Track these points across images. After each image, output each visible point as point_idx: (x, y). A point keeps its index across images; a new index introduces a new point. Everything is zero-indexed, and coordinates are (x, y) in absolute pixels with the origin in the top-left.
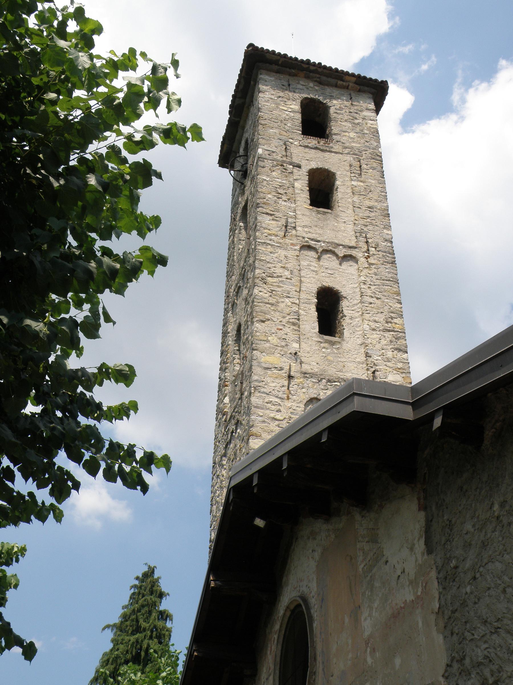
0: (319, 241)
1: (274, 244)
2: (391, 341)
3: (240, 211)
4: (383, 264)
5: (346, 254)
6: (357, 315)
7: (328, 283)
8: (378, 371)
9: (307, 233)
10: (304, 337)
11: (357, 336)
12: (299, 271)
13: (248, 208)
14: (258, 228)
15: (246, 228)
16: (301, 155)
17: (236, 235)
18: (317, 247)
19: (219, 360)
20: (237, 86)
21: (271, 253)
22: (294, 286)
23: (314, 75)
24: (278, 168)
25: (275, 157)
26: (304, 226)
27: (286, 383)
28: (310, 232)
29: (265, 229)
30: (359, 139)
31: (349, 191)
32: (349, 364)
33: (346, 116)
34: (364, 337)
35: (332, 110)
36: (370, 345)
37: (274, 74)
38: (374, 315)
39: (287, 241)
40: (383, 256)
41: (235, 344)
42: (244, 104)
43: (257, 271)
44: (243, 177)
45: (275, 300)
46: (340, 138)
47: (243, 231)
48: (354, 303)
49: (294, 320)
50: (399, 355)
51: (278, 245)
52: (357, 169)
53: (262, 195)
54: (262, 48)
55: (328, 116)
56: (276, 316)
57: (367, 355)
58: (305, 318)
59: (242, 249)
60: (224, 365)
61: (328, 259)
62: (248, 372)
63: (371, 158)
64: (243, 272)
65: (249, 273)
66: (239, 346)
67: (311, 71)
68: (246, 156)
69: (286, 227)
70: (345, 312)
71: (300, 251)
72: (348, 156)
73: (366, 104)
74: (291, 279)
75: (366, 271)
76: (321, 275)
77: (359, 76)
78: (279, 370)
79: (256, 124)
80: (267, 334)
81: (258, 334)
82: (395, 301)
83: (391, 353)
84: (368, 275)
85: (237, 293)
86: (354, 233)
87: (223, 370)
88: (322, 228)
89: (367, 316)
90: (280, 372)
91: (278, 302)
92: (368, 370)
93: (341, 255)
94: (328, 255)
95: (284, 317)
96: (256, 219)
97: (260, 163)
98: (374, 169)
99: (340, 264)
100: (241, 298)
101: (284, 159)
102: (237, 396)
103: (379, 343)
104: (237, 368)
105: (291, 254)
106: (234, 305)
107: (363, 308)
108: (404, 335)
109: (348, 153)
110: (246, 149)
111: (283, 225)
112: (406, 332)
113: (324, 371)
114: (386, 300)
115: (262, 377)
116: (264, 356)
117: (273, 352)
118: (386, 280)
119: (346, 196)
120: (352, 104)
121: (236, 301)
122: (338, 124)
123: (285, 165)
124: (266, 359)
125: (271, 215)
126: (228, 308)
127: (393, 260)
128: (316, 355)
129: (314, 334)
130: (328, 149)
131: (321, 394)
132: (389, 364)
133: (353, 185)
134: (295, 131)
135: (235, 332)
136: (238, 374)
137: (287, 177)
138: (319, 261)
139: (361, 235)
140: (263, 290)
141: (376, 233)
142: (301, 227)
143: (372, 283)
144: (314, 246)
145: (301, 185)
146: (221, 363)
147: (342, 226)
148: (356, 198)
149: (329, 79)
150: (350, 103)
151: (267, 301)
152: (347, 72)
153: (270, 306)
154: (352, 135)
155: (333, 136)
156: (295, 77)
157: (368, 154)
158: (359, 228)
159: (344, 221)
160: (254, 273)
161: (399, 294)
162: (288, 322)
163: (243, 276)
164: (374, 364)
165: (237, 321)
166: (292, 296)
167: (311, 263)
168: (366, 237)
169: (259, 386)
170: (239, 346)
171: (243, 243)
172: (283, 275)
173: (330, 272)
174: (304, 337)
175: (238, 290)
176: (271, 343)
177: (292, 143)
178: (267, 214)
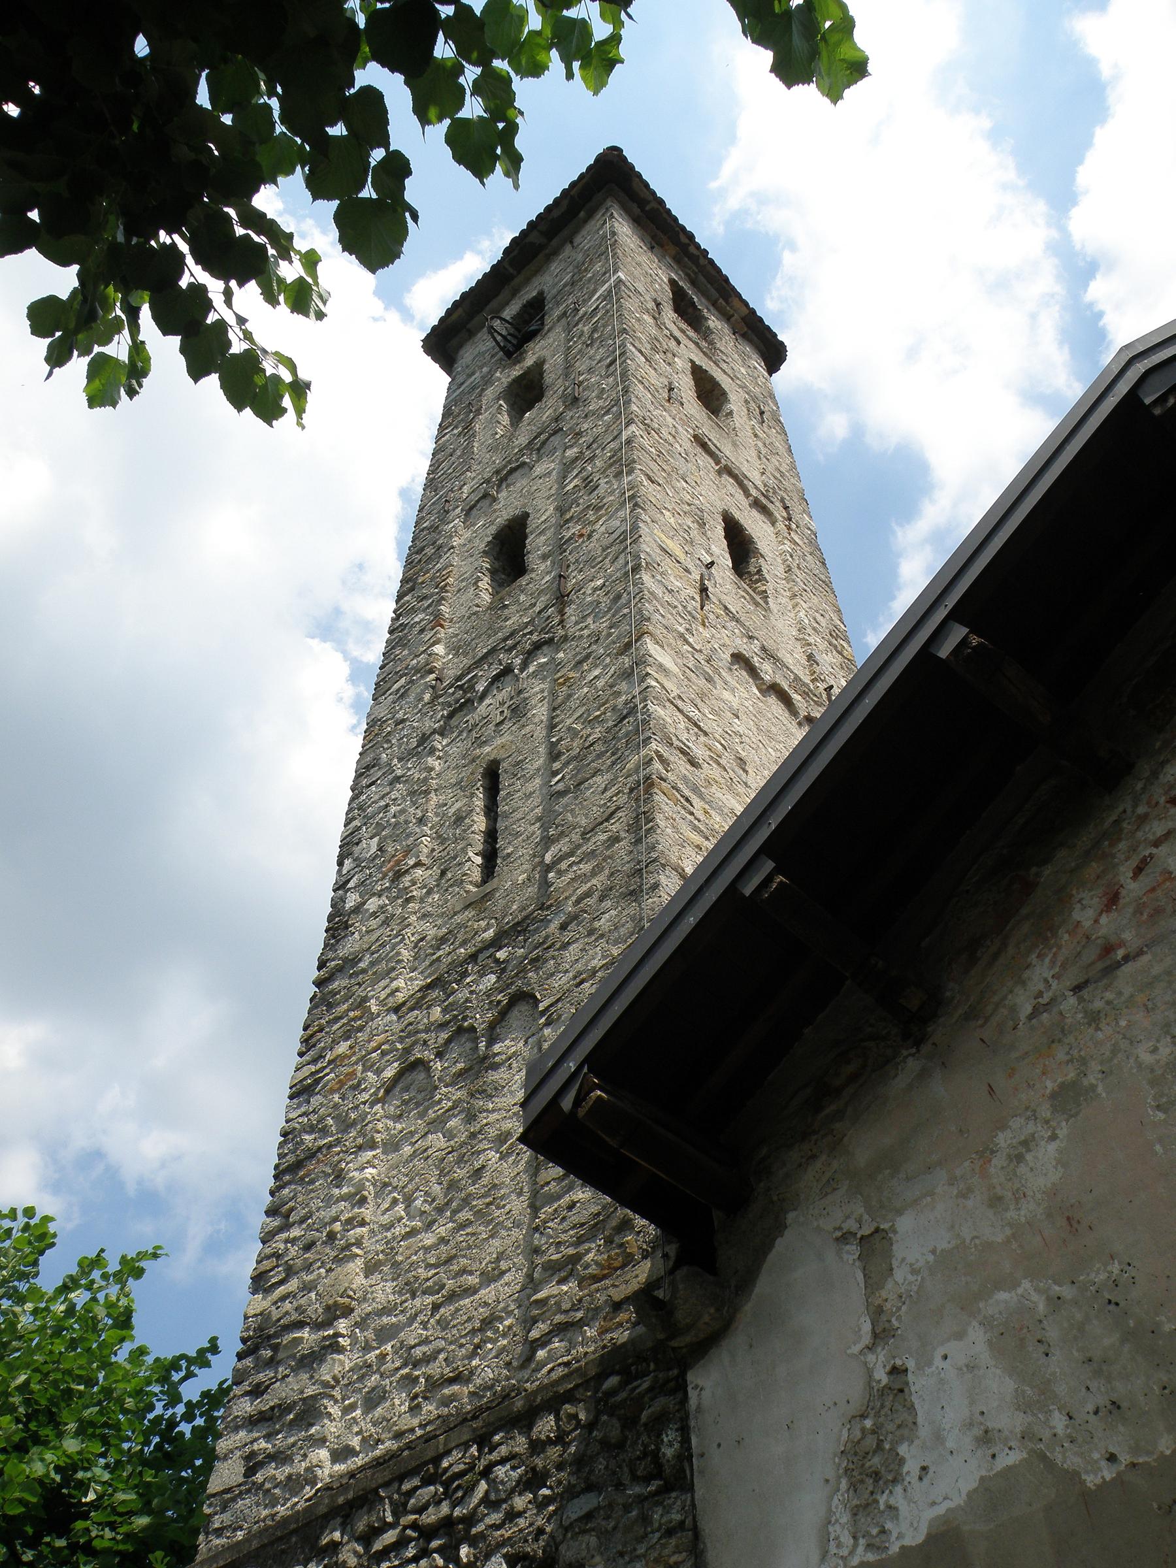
42: (541, 247)
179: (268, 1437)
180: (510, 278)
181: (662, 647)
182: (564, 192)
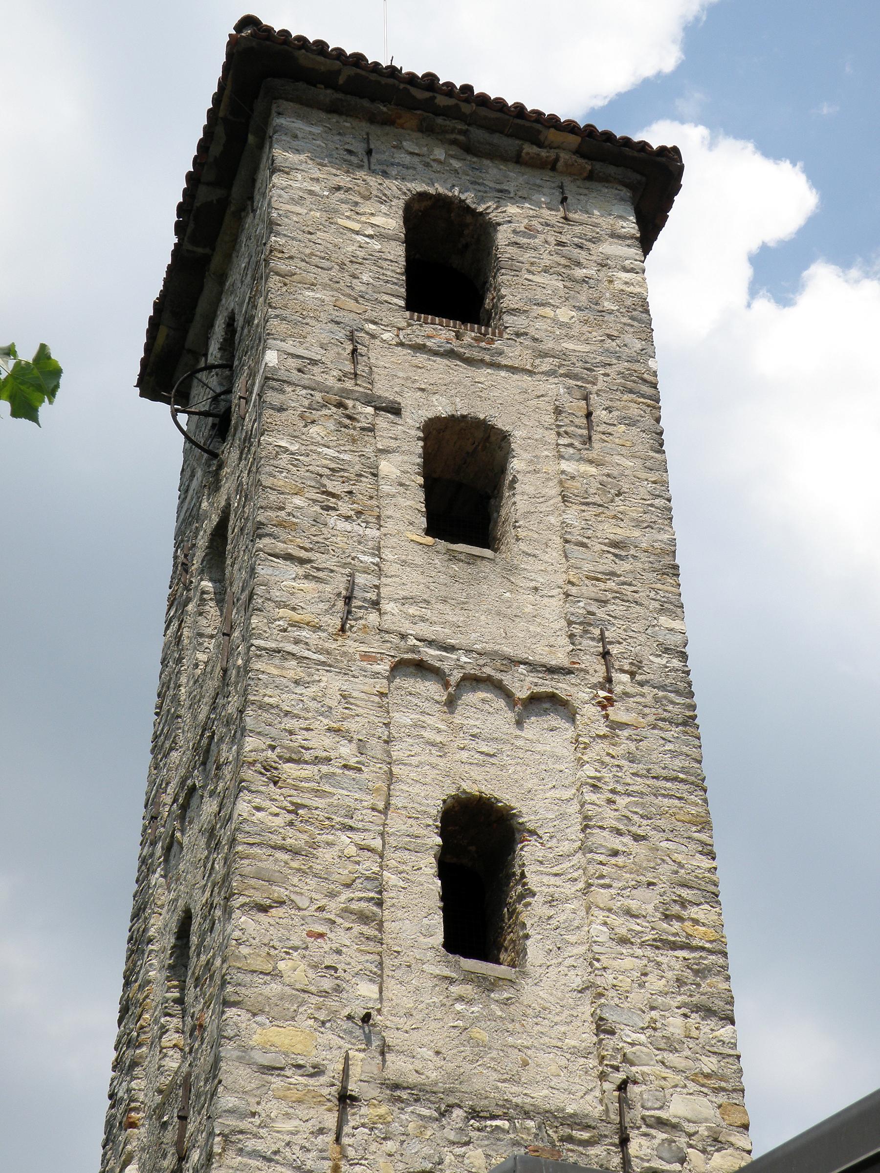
0: (451, 649)
1: (306, 654)
2: (680, 982)
3: (202, 541)
4: (654, 727)
5: (536, 690)
6: (570, 889)
7: (480, 782)
8: (635, 1082)
9: (414, 620)
10: (396, 962)
11: (570, 962)
12: (386, 742)
13: (230, 536)
14: (258, 601)
15: (220, 598)
16: (401, 374)
17: (189, 620)
18: (446, 666)
19: (113, 1031)
20: (203, 146)
21: (297, 683)
22: (369, 791)
23: (449, 123)
24: (327, 412)
25: (319, 378)
26: (405, 600)
27: (331, 1120)
28: (423, 619)
29: (280, 605)
30: (585, 328)
31: (553, 490)
32: (543, 1058)
33: (545, 256)
34: (591, 965)
35: (503, 236)
36: (612, 993)
37: (323, 115)
38: (626, 892)
39: (351, 646)
40: (657, 699)
41: (168, 979)
42: (224, 203)
43: (251, 743)
44: (216, 435)
45: (305, 837)
46: (526, 322)
47: (212, 608)
48: (560, 850)
49: (363, 905)
50: (706, 1030)
51: (322, 658)
52: (577, 421)
53: (273, 497)
54: (285, 33)
55: (489, 254)
56: (307, 892)
57: (603, 1028)
58: (402, 899)
59: (206, 664)
60: (130, 1052)
61: (480, 705)
62: (206, 1080)
63: (622, 389)
64: (205, 741)
65: (224, 747)
66: (182, 989)
67: (439, 112)
68: (228, 367)
69: (348, 600)
70: (533, 881)
71: (390, 679)
72: (552, 380)
73: (611, 220)
74: (360, 770)
75: (599, 748)
76: (457, 757)
77: (590, 130)
78: (311, 1076)
79: (259, 273)
80: (273, 952)
81: (244, 950)
82: (692, 846)
83: (679, 1021)
84: (607, 759)
85: (185, 807)
86: (564, 623)
87: (124, 1067)
88: (463, 605)
89: (602, 896)
90: (312, 1081)
91: (314, 845)
92: (603, 1076)
93: (522, 694)
94: (482, 695)
95: (332, 895)
96: (252, 572)
97: (272, 397)
98: (631, 423)
99: (519, 723)
100: (196, 827)
101: (349, 384)
102: (165, 1163)
103: (642, 985)
104: (173, 1063)
105: (362, 687)
106: (171, 847)
107: (591, 869)
108: (721, 961)
109: (552, 373)
110: (229, 345)
111: (339, 595)
112: (728, 950)
113: (460, 1078)
114: (664, 844)
115: (253, 1100)
116: (260, 1025)
117: (291, 1014)
118: (666, 779)
119: (543, 508)
120: (565, 218)
121: (178, 834)
122: (521, 280)
123: (350, 403)
124: (266, 1036)
125: (302, 561)
126: (152, 855)
127: (688, 713)
128: (434, 1025)
129: (430, 954)
130: (487, 358)
131: (447, 1161)
132: (672, 1058)
133: (563, 472)
134: (386, 298)
135: (170, 940)
136: (172, 1086)
137: (354, 441)
138: (452, 713)
139: (586, 632)
140: (267, 804)
141: (634, 627)
142: (396, 600)
143: (619, 788)
144: (438, 664)
145: (400, 469)
146: (119, 1042)
147: (527, 602)
148: (572, 515)
149: (497, 139)
150: (561, 213)
151: (277, 839)
152: (553, 118)
153: (286, 857)
154: (565, 314)
155: (506, 317)
156: (387, 128)
157: (613, 375)
158: (579, 609)
159: (533, 584)
160: (240, 748)
161: (705, 825)
162: (346, 910)
163: (204, 755)
164: (625, 1059)
165: (181, 903)
166: (360, 825)
167: (426, 718)
168: (602, 638)
169: (241, 1132)
170: (182, 989)
171: (211, 644)
172: (333, 754)
173: (485, 749)
174: (396, 962)
175: (188, 798)
176: (287, 980)
177: (373, 336)
178: (289, 557)
179: (236, 296)
180: (206, 260)
181: (225, 863)
182: (211, 113)
